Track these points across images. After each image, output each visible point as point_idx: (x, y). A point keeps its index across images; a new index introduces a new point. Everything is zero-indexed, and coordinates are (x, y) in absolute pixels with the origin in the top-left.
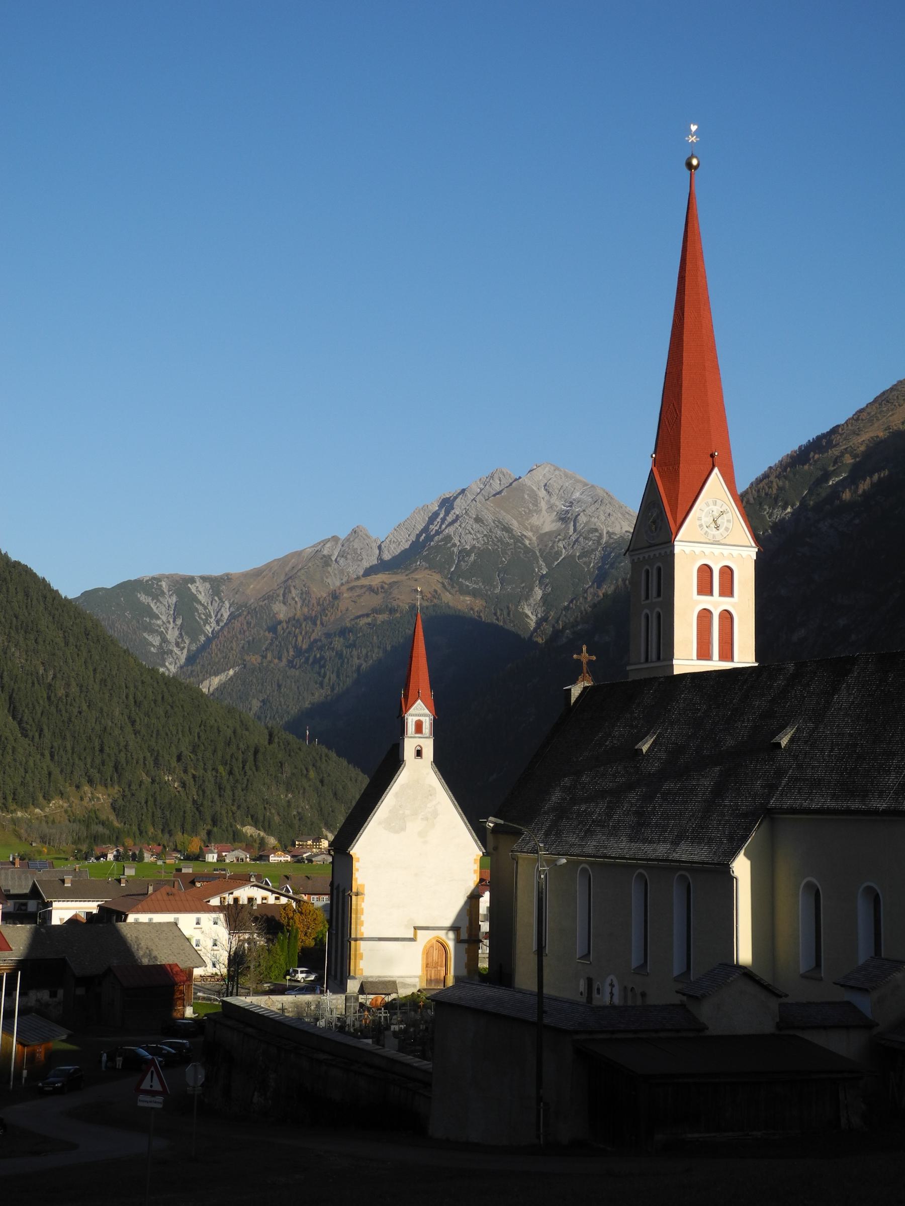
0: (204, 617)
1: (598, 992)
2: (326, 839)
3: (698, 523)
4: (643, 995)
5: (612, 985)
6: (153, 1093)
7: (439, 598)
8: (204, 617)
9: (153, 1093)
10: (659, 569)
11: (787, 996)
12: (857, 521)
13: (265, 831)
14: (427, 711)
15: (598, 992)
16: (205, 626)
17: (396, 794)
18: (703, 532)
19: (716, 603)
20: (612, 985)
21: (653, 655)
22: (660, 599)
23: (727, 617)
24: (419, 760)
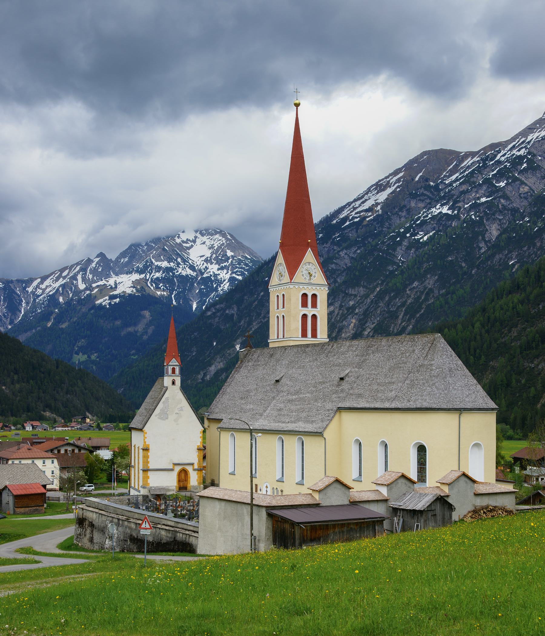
0: (18, 301)
1: (261, 491)
2: (88, 418)
3: (302, 274)
4: (282, 491)
5: (267, 487)
6: (146, 529)
7: (145, 291)
8: (18, 301)
9: (146, 529)
10: (284, 295)
11: (353, 488)
12: (359, 251)
13: (56, 414)
14: (177, 364)
15: (261, 491)
16: (19, 306)
17: (163, 403)
18: (303, 278)
19: (309, 311)
20: (267, 487)
21: (281, 336)
22: (284, 309)
23: (314, 317)
24: (174, 386)
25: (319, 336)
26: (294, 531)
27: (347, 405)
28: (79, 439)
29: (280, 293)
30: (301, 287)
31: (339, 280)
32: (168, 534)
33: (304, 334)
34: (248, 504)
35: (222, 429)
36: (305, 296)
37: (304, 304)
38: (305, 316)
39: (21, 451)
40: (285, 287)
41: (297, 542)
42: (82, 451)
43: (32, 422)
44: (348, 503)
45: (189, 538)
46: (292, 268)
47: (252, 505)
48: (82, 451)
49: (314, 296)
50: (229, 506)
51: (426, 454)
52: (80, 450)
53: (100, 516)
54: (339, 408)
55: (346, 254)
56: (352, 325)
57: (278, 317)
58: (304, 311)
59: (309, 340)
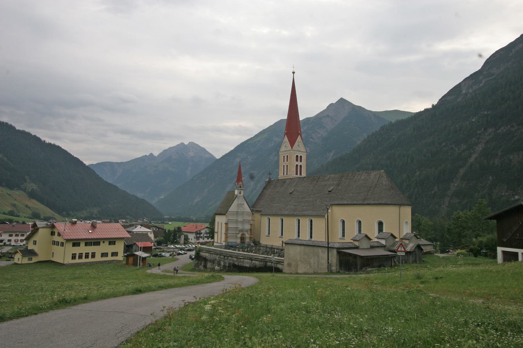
19: (299, 163)
22: (288, 162)
23: (301, 166)
25: (302, 175)
26: (356, 261)
27: (336, 202)
28: (141, 228)
29: (285, 155)
30: (296, 152)
31: (247, 167)
32: (261, 263)
33: (297, 174)
34: (326, 247)
35: (262, 215)
36: (297, 156)
37: (297, 160)
38: (297, 165)
39: (137, 228)
40: (288, 152)
41: (359, 267)
42: (160, 230)
43: (122, 220)
44: (369, 247)
45: (276, 265)
46: (292, 144)
47: (328, 247)
48: (160, 230)
49: (301, 157)
50: (307, 249)
51: (361, 230)
52: (159, 229)
53: (211, 255)
54: (331, 204)
55: (250, 157)
56: (252, 185)
57: (284, 166)
58: (297, 163)
59: (299, 176)
